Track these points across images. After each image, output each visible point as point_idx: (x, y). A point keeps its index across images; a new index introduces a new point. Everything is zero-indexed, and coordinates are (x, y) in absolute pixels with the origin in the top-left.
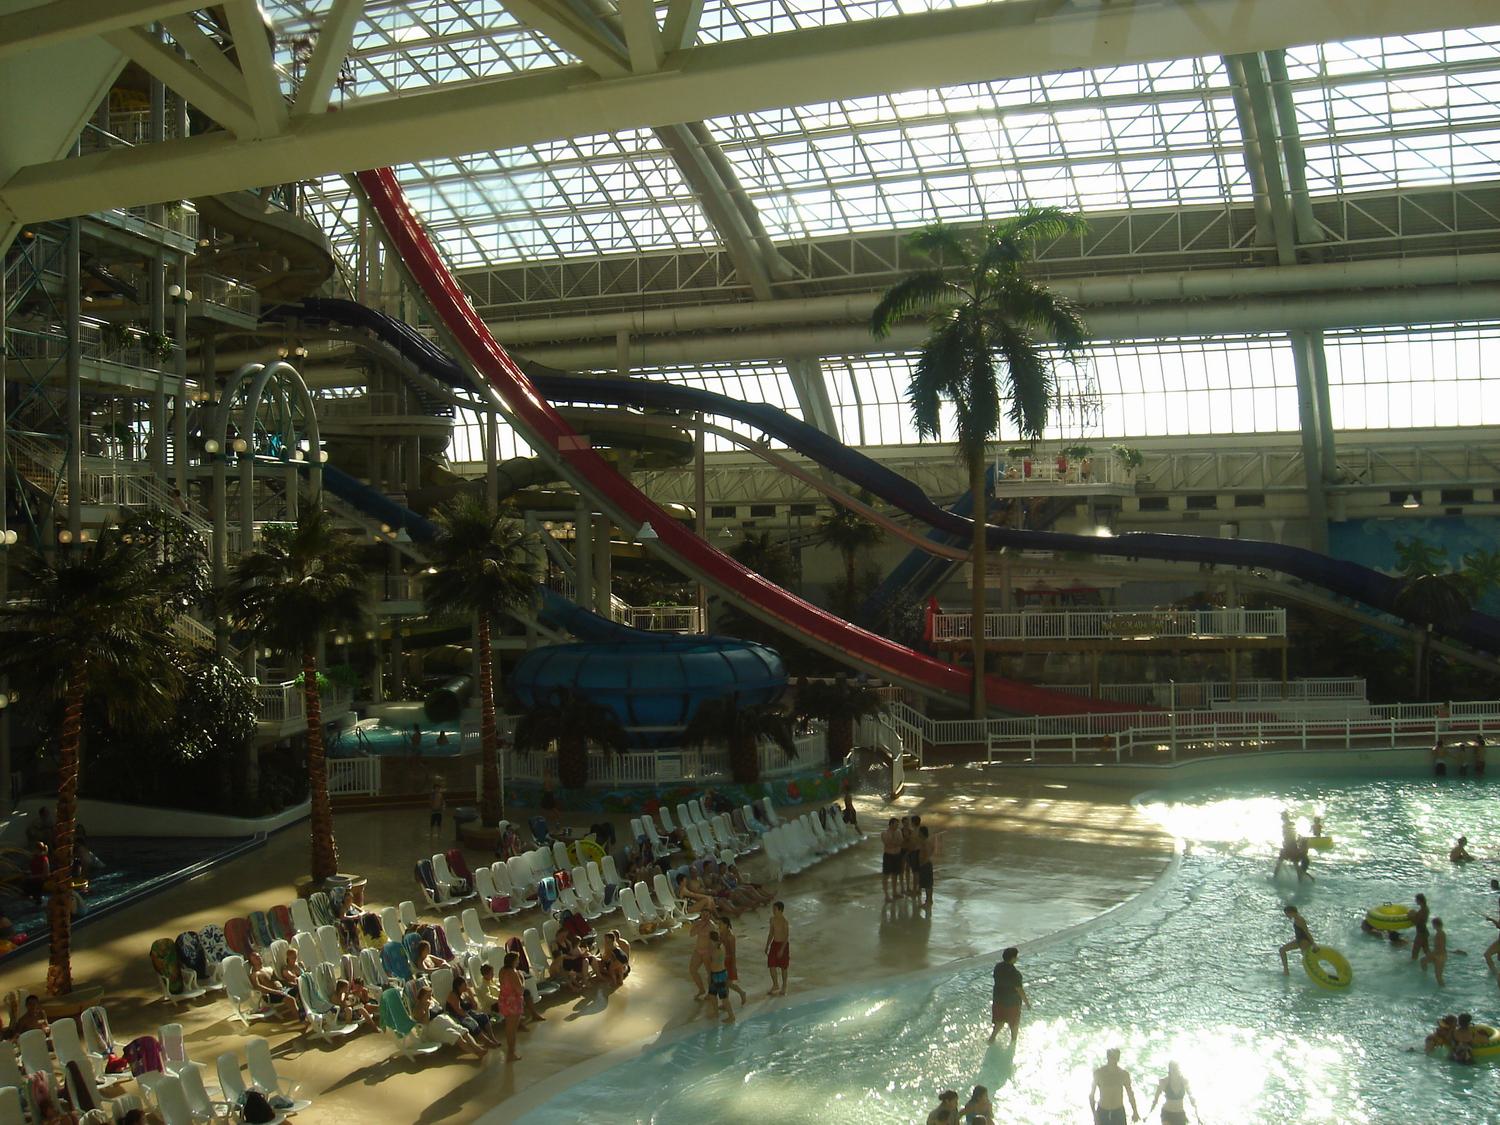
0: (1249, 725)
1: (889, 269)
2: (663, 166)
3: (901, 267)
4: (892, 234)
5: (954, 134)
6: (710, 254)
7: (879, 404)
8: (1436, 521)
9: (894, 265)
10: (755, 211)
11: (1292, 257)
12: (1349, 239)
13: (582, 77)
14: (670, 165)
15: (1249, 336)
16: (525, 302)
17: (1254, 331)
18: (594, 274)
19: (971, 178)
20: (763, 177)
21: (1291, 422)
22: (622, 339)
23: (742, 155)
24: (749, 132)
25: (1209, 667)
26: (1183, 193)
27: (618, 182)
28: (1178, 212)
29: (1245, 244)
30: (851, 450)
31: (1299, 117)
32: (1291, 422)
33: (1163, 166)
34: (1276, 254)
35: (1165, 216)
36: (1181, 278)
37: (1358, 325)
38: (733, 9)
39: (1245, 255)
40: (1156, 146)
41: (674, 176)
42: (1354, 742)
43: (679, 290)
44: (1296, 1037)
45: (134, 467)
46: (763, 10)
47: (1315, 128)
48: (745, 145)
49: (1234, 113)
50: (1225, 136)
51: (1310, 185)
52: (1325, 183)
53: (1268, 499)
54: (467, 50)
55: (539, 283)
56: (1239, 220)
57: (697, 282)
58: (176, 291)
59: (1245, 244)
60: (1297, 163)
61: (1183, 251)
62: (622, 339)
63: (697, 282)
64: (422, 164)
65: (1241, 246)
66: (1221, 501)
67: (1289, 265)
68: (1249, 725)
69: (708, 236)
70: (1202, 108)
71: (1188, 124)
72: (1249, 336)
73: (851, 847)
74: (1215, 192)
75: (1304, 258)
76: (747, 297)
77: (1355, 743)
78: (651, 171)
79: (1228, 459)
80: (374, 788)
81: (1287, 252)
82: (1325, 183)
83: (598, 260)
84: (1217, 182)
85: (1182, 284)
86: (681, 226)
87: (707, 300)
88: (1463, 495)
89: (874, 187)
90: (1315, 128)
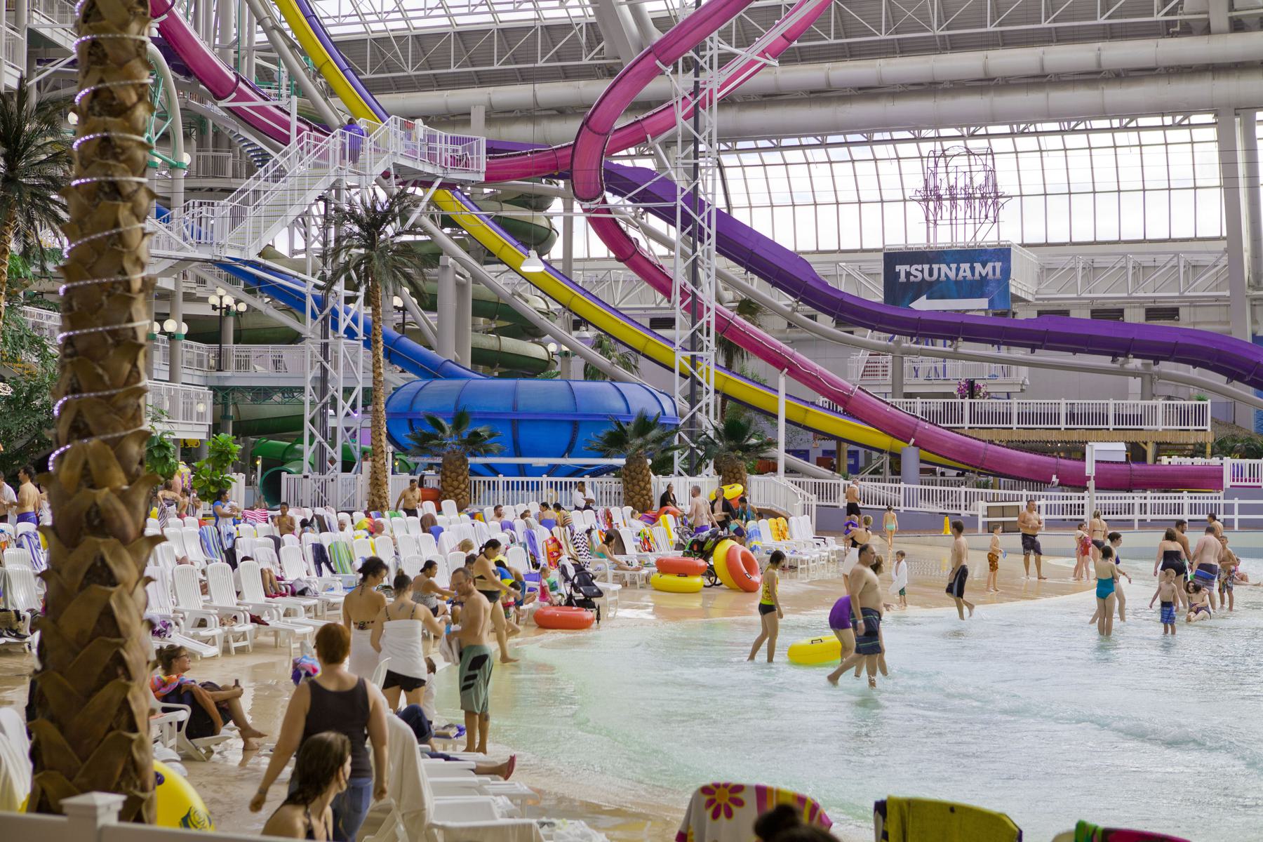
0: (1217, 502)
7: (882, 201)
9: (829, 35)
11: (1225, 24)
15: (1116, 123)
17: (1182, 111)
21: (1212, 222)
22: (478, 117)
25: (59, 220)
28: (538, 24)
29: (1173, 12)
32: (1212, 222)
34: (1208, 22)
39: (1174, 23)
43: (540, 64)
44: (142, 339)
45: (392, 242)
55: (383, 56)
57: (558, 57)
59: (1173, 12)
61: (1101, 21)
62: (478, 117)
63: (558, 57)
65: (1166, 14)
67: (1220, 32)
68: (1217, 502)
72: (1116, 123)
75: (1238, 26)
81: (1220, 19)
83: (450, 30)
87: (566, 75)
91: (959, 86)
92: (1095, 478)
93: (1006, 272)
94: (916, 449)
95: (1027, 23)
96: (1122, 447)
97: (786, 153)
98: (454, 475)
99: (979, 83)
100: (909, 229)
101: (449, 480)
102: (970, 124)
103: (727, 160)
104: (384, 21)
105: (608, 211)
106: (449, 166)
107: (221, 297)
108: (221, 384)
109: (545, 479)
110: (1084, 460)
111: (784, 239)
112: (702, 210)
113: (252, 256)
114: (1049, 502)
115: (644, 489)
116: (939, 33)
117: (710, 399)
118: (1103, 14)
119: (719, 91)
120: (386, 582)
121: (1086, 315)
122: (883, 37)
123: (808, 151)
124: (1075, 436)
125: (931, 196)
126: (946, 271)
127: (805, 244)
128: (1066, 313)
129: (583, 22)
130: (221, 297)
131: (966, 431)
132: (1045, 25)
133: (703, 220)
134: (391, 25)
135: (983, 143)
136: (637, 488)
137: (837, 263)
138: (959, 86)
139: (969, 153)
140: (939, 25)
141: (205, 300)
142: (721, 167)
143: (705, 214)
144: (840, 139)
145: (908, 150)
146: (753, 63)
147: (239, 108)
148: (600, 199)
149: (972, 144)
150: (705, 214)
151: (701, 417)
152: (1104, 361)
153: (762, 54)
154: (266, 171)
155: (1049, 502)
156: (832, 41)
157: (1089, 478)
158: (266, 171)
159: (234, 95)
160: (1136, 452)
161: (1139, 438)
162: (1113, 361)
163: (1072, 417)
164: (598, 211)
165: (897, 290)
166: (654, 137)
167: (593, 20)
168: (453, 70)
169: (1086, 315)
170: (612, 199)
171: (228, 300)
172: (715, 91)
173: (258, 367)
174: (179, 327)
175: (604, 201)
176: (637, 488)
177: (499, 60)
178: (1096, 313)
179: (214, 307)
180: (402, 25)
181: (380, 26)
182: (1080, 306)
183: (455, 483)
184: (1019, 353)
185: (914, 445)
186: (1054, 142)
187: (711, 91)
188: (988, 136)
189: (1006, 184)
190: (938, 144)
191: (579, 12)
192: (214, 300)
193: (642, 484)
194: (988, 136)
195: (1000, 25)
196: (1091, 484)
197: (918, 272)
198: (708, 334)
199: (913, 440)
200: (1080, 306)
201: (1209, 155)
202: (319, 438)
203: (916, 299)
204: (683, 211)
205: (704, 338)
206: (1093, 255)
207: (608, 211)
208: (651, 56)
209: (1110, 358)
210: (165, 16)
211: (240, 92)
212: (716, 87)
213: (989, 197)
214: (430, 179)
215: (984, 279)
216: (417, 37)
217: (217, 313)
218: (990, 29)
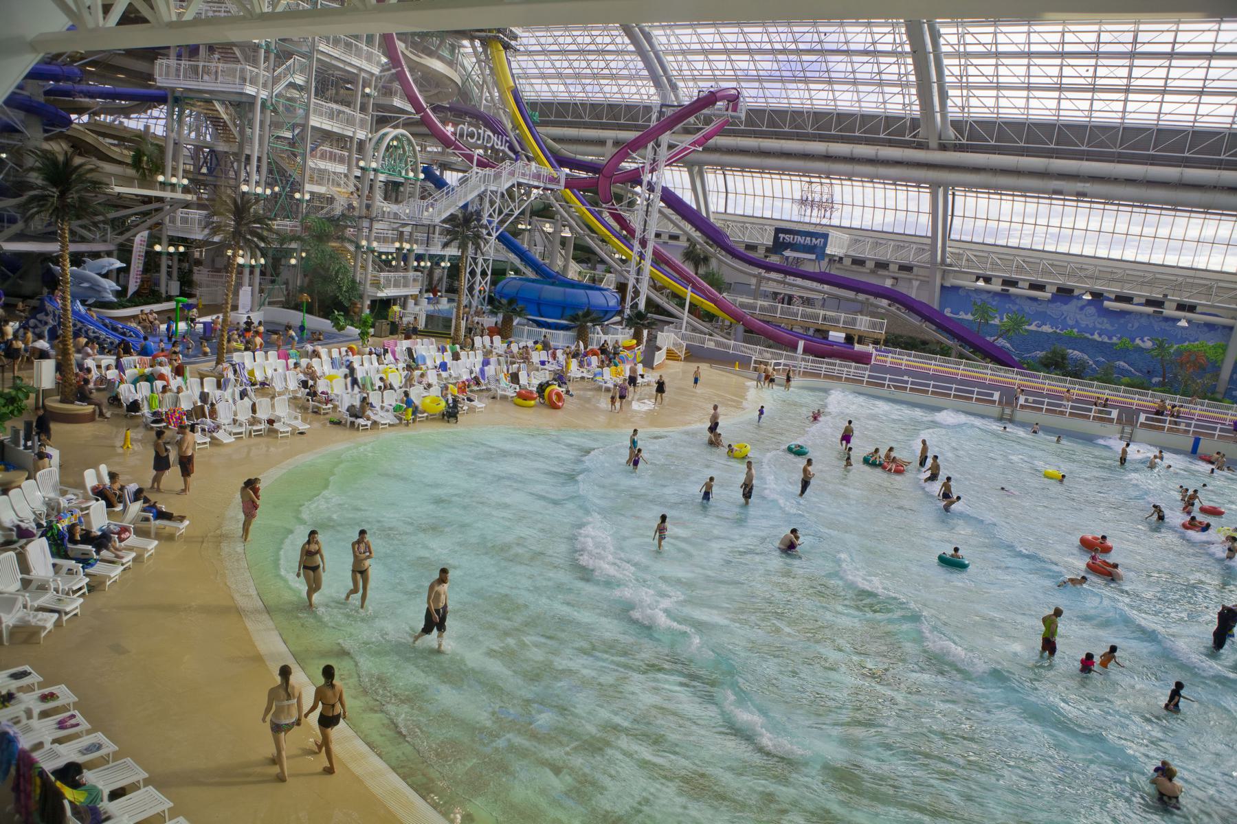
8: (996, 294)
13: (244, 18)
22: (609, 143)
23: (671, 58)
24: (676, 47)
26: (1095, 114)
27: (699, 63)
31: (947, 72)
37: (969, 187)
41: (641, 65)
42: (955, 396)
43: (882, 136)
47: (953, 79)
48: (674, 53)
51: (950, 109)
52: (957, 110)
53: (915, 269)
56: (915, 123)
58: (367, 90)
59: (914, 136)
60: (944, 96)
64: (661, 36)
65: (889, 134)
66: (892, 267)
69: (655, 97)
71: (891, 69)
73: (176, 246)
74: (900, 107)
75: (943, 147)
76: (921, 146)
77: (955, 396)
79: (778, 231)
80: (421, 325)
81: (933, 143)
82: (957, 110)
84: (901, 103)
87: (822, 138)
88: (1014, 283)
90: (953, 79)
93: (825, 244)
96: (843, 335)
100: (789, 213)
120: (1062, 466)
124: (824, 328)
126: (799, 239)
139: (821, 184)
146: (686, 149)
153: (693, 144)
160: (849, 339)
161: (852, 333)
163: (825, 318)
165: (778, 247)
190: (946, 62)
197: (789, 238)
201: (926, 206)
203: (791, 247)
206: (879, 237)
213: (827, 205)
215: (815, 246)
216: (592, 105)
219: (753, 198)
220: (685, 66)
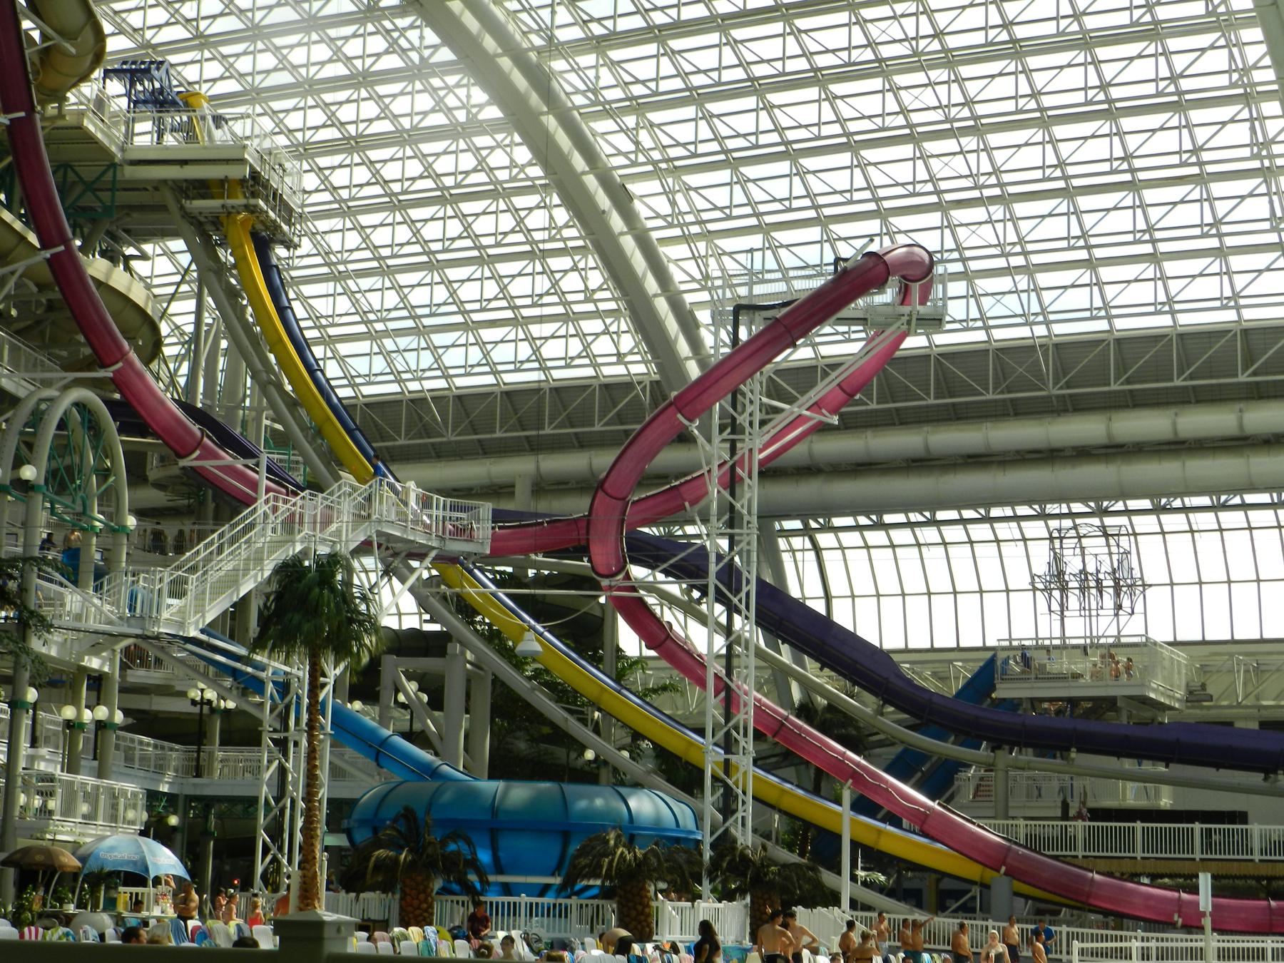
1: (923, 399)
2: (613, 328)
3: (878, 403)
4: (814, 363)
5: (1011, 219)
6: (639, 383)
10: (630, 197)
12: (936, 398)
14: (591, 263)
16: (402, 442)
18: (541, 401)
19: (971, 284)
20: (707, 277)
23: (605, 125)
30: (796, 600)
33: (1215, 268)
35: (1097, 343)
36: (1241, 411)
38: (929, 13)
40: (1159, 94)
43: (598, 427)
46: (974, 17)
48: (608, 111)
49: (1263, 48)
50: (1258, 76)
54: (341, 103)
55: (421, 418)
57: (620, 419)
61: (1243, 378)
63: (620, 419)
65: (1249, 376)
70: (1263, 189)
78: (492, 149)
85: (538, 468)
86: (603, 346)
89: (964, 283)
91: (1083, 453)
92: (1211, 914)
94: (1006, 879)
95: (1157, 381)
97: (893, 533)
98: (414, 892)
99: (1103, 451)
101: (408, 898)
102: (1098, 500)
103: (825, 539)
104: (420, 379)
105: (634, 589)
106: (447, 536)
107: (202, 690)
108: (198, 793)
109: (524, 899)
110: (1197, 893)
111: (868, 633)
112: (738, 590)
113: (193, 633)
114: (1160, 944)
115: (642, 913)
116: (1056, 392)
117: (747, 810)
118: (1244, 371)
119: (761, 451)
121: (1254, 725)
122: (990, 396)
123: (917, 530)
125: (1057, 579)
127: (892, 641)
128: (1231, 724)
129: (647, 380)
130: (202, 690)
131: (1080, 862)
132: (1178, 383)
133: (740, 601)
134: (429, 385)
135: (1123, 520)
136: (634, 913)
137: (950, 662)
138: (1083, 453)
140: (1055, 384)
141: (183, 694)
142: (817, 549)
143: (743, 595)
144: (1008, 512)
145: (1035, 529)
146: (799, 419)
147: (202, 468)
148: (620, 577)
149: (1108, 521)
150: (743, 595)
151: (737, 832)
152: (1256, 778)
154: (221, 536)
155: (1160, 944)
156: (932, 401)
157: (1203, 914)
158: (221, 536)
159: (197, 453)
162: (1265, 779)
164: (620, 589)
166: (692, 504)
167: (657, 377)
168: (498, 434)
169: (1254, 725)
170: (638, 572)
171: (211, 695)
172: (756, 452)
173: (226, 772)
174: (112, 714)
175: (628, 577)
176: (634, 913)
177: (550, 423)
178: (1265, 725)
179: (194, 702)
180: (442, 384)
181: (413, 386)
182: (1246, 718)
183: (416, 903)
184: (1128, 764)
185: (1005, 874)
186: (1204, 520)
187: (751, 450)
188: (1127, 512)
189: (1154, 571)
191: (641, 369)
192: (195, 694)
193: (640, 908)
194: (1127, 512)
195: (1128, 382)
196: (1207, 922)
198: (745, 735)
199: (1003, 869)
200: (1246, 718)
202: (274, 850)
204: (716, 587)
205: (740, 738)
207: (634, 589)
208: (673, 407)
209: (1262, 775)
210: (120, 365)
211: (205, 448)
212: (758, 443)
213: (1125, 584)
214: (423, 551)
217: (196, 710)
218: (1114, 387)
219: (929, 587)
220: (606, 78)
